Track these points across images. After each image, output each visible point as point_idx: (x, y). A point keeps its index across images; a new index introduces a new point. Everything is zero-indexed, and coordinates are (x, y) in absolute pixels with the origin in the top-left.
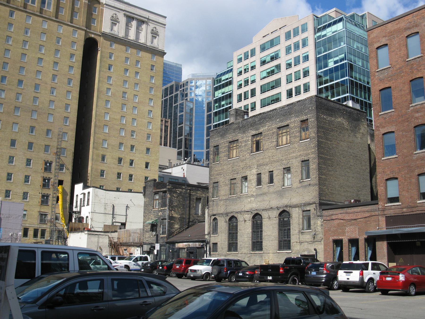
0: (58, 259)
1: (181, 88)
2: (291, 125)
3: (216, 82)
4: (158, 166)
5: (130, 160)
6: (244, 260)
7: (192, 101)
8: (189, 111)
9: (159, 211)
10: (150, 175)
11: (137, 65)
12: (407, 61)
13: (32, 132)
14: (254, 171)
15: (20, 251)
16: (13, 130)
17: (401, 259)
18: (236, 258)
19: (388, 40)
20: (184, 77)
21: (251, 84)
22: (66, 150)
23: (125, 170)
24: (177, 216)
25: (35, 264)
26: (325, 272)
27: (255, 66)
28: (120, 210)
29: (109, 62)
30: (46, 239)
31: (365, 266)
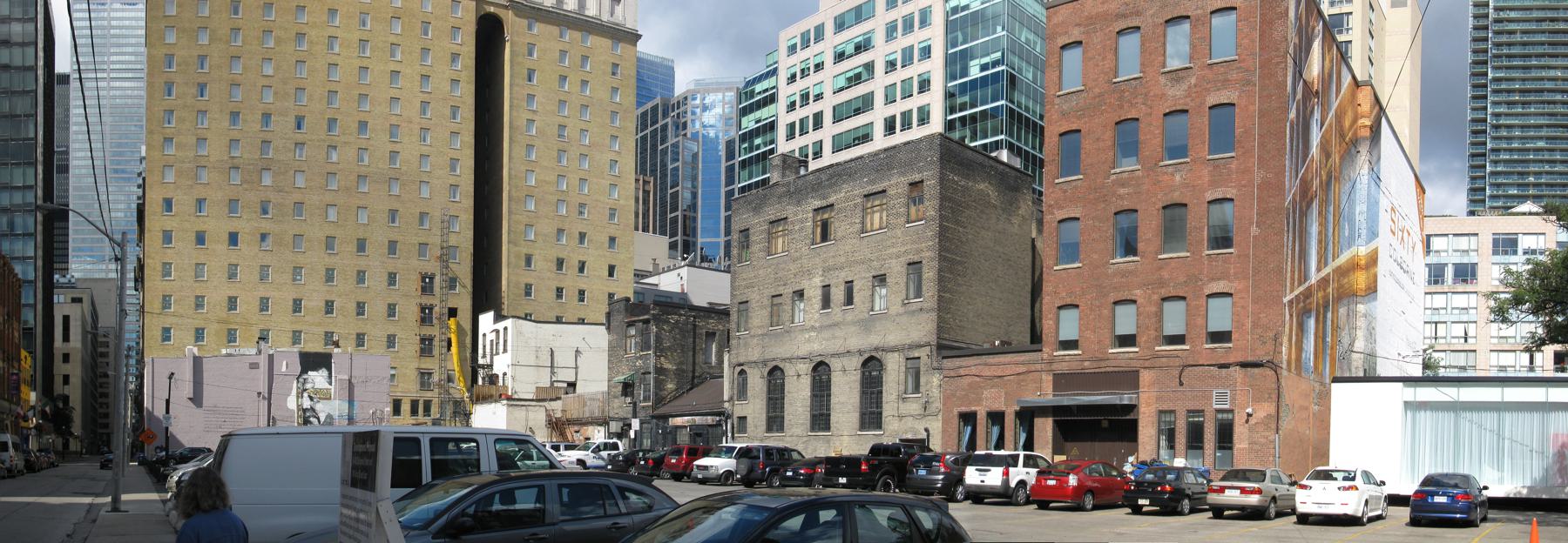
0: (460, 451)
1: (673, 111)
2: (891, 192)
3: (743, 96)
5: (580, 261)
6: (795, 448)
7: (695, 137)
8: (689, 159)
9: (637, 358)
10: (616, 289)
11: (583, 65)
12: (1115, 83)
13: (393, 221)
14: (818, 281)
15: (396, 439)
16: (360, 222)
17: (1075, 449)
18: (781, 445)
20: (680, 89)
21: (814, 101)
23: (571, 281)
24: (670, 366)
25: (420, 461)
26: (942, 470)
27: (823, 62)
28: (564, 359)
29: (529, 63)
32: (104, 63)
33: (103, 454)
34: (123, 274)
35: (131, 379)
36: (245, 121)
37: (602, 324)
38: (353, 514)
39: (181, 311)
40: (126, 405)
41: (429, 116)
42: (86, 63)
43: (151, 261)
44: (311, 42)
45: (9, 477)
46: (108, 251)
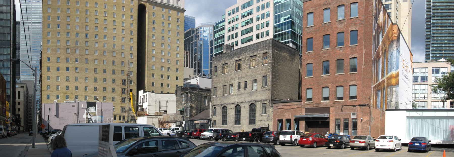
0: (133, 130)
1: (195, 32)
2: (258, 55)
3: (215, 28)
4: (183, 79)
5: (168, 76)
6: (230, 130)
7: (201, 40)
8: (200, 46)
9: (185, 104)
11: (169, 19)
12: (323, 24)
13: (114, 64)
14: (237, 81)
15: (115, 127)
17: (311, 130)
18: (226, 129)
19: (314, 10)
20: (197, 26)
21: (236, 29)
22: (133, 72)
23: (165, 81)
25: (122, 133)
26: (273, 136)
27: (238, 18)
28: (163, 104)
29: (153, 18)
30: (125, 121)
31: (293, 133)
32: (30, 18)
33: (30, 131)
34: (36, 79)
35: (38, 110)
36: (71, 35)
37: (174, 94)
38: (102, 149)
39: (52, 90)
40: (36, 117)
41: (124, 33)
42: (25, 18)
43: (44, 75)
44: (90, 12)
45: (3, 138)
46: (31, 73)
